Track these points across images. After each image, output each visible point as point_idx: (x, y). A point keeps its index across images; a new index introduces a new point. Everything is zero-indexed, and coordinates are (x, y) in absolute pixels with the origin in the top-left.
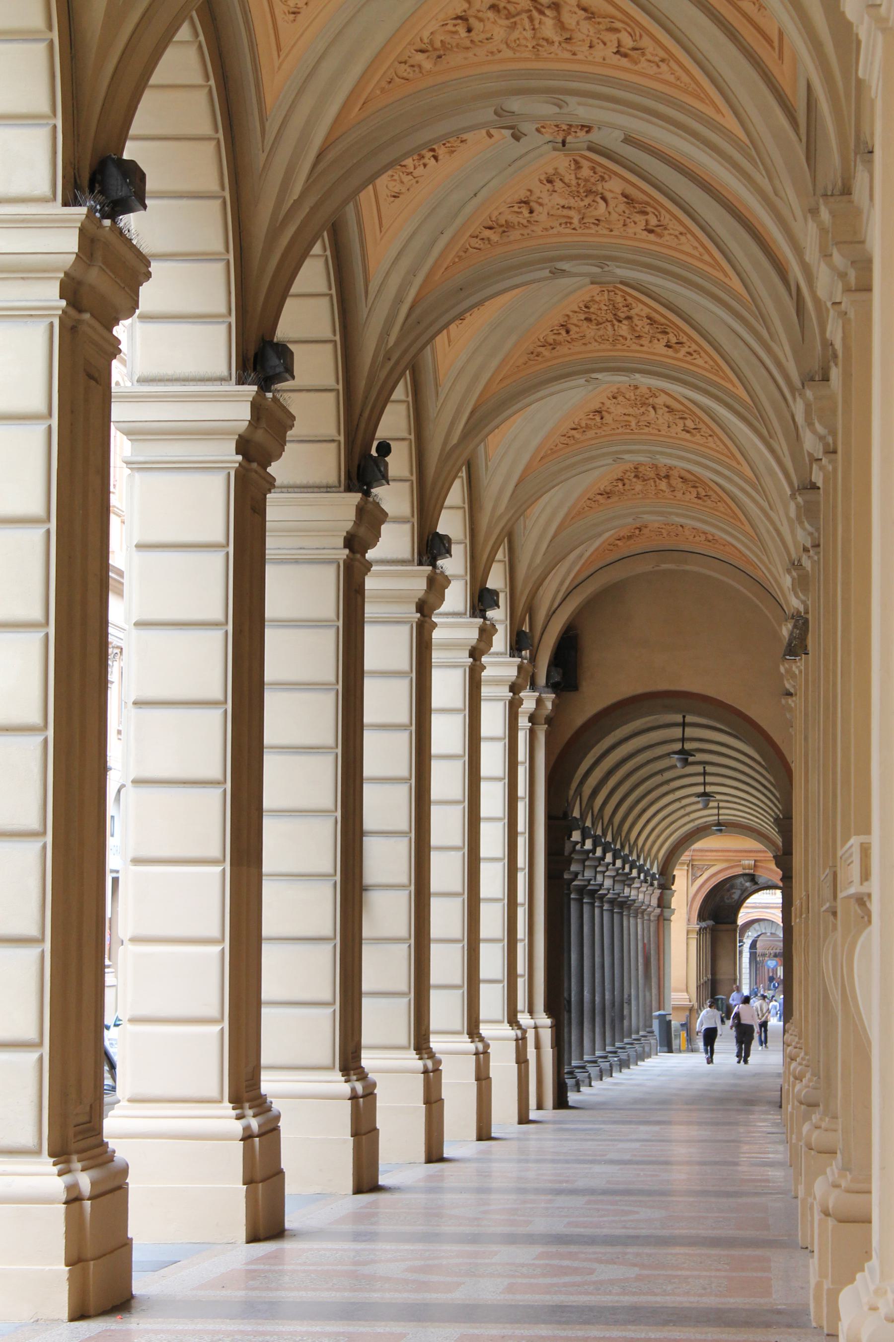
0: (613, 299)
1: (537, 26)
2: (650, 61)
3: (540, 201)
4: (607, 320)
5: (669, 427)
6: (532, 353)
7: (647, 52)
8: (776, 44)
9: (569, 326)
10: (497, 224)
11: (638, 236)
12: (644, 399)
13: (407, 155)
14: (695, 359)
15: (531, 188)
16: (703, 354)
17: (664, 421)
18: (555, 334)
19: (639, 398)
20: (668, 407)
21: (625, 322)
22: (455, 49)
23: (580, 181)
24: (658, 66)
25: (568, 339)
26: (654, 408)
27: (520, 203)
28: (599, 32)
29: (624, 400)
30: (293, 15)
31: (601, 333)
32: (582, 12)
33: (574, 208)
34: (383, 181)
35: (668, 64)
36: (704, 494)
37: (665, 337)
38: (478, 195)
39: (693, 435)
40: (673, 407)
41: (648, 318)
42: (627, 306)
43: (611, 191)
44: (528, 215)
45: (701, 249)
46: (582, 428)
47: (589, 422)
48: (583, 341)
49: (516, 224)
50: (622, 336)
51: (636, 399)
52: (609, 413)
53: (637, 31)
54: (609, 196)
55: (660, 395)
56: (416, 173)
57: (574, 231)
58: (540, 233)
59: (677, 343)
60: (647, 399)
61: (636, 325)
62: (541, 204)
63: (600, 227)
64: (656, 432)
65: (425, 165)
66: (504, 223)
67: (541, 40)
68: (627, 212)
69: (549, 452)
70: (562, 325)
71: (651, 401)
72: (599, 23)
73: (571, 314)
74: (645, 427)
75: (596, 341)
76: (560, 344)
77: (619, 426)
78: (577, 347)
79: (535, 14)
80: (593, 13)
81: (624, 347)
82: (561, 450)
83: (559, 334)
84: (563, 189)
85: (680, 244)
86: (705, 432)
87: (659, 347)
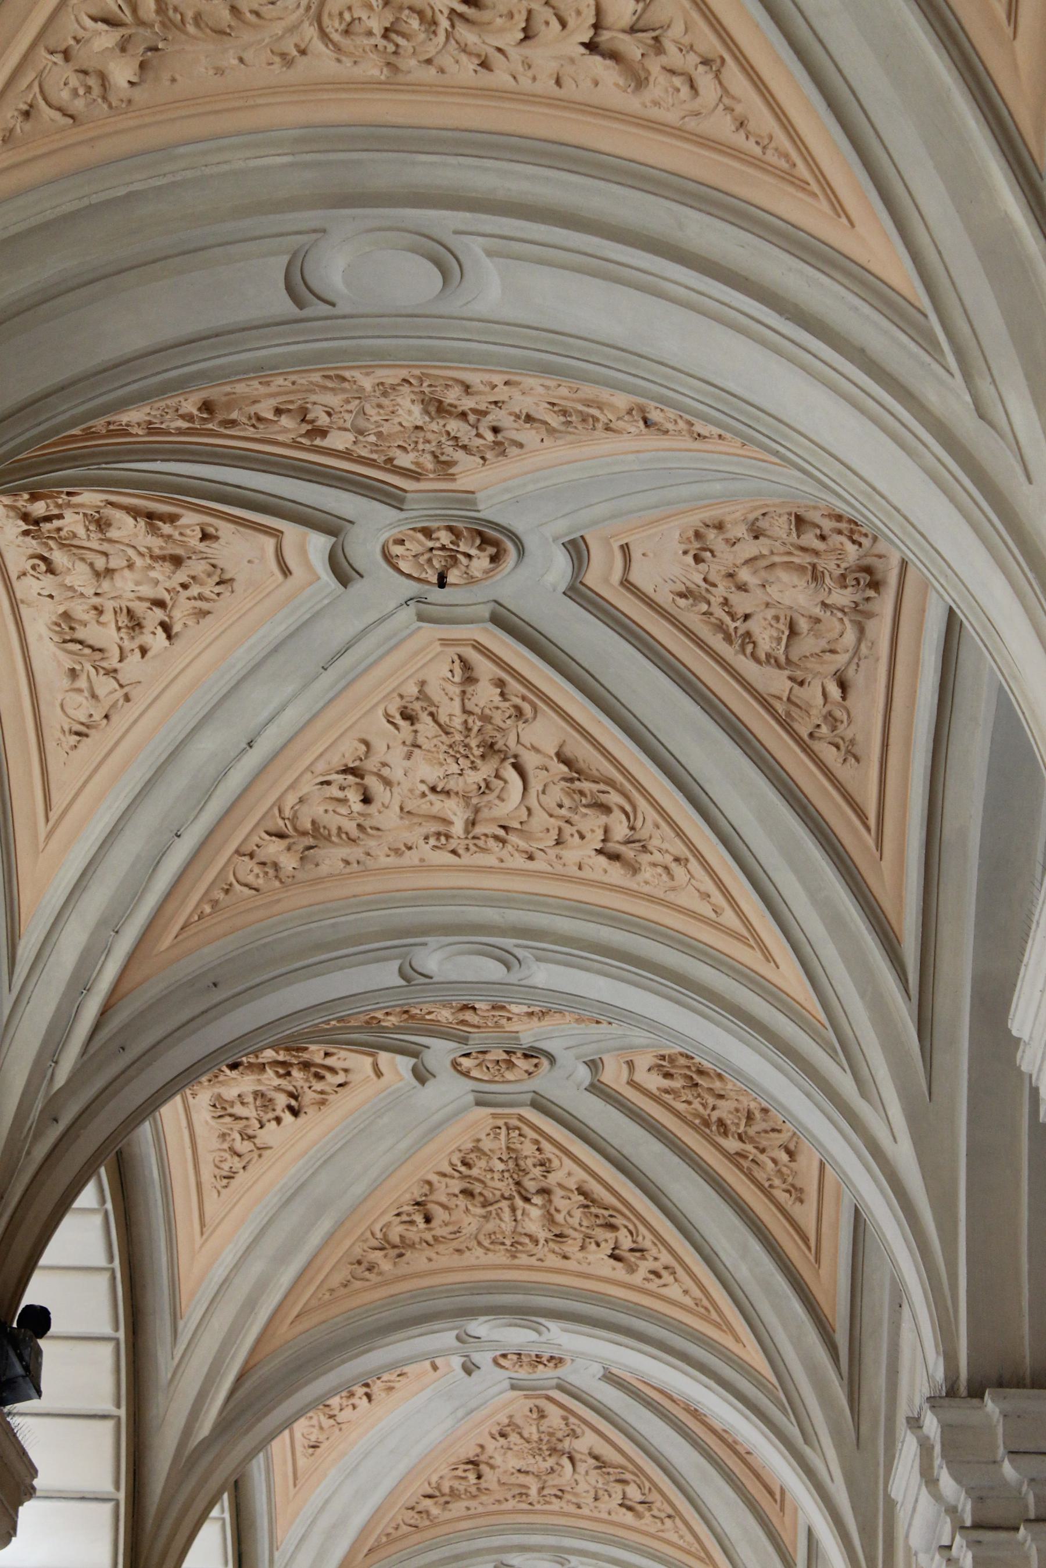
0: (518, 1146)
1: (519, 1217)
2: (654, 1516)
3: (386, 772)
4: (503, 1197)
5: (596, 1499)
6: (359, 1263)
7: (654, 1507)
8: (872, 822)
9: (430, 1206)
10: (295, 829)
11: (587, 873)
12: (554, 1439)
13: (333, 1392)
14: (665, 1285)
15: (368, 738)
16: (680, 1272)
17: (587, 1487)
18: (405, 1222)
19: (546, 1438)
20: (596, 1458)
21: (537, 1200)
22: (191, 29)
23: (543, 1436)
24: (663, 1523)
25: (428, 1237)
26: (571, 1459)
27: (467, 1463)
28: (607, 1483)
29: (520, 1441)
30: (78, 738)
31: (490, 1226)
32: (594, 1461)
33: (457, 793)
34: (301, 1426)
35: (717, 75)
36: (639, 1497)
37: (610, 1235)
38: (255, 745)
39: (639, 1516)
40: (605, 1458)
41: (581, 1191)
42: (542, 1165)
43: (534, 748)
44: (475, 1481)
45: (718, 898)
46: (443, 1495)
47: (456, 1484)
48: (455, 1244)
49: (334, 831)
50: (530, 1236)
51: (541, 1440)
52: (492, 1467)
53: (647, 1485)
54: (530, 761)
55: (583, 1433)
56: (264, 1136)
57: (530, 1507)
58: (384, 861)
59: (632, 1250)
60: (560, 1440)
61: (557, 1211)
62: (387, 782)
63: (564, 1501)
64: (572, 1509)
65: (354, 1407)
66: (308, 826)
67: (407, 12)
68: (567, 802)
69: (384, 1539)
70: (418, 1204)
71: (566, 1444)
72: (609, 1474)
73: (434, 1178)
74: (554, 1500)
75: (479, 1244)
76: (412, 1246)
77: (509, 1496)
78: (445, 1258)
79: (519, 1202)
80: (603, 1462)
81: (533, 1261)
82: (405, 1536)
83: (412, 1222)
84: (435, 741)
85: (673, 889)
86: (659, 1510)
87: (598, 1260)
